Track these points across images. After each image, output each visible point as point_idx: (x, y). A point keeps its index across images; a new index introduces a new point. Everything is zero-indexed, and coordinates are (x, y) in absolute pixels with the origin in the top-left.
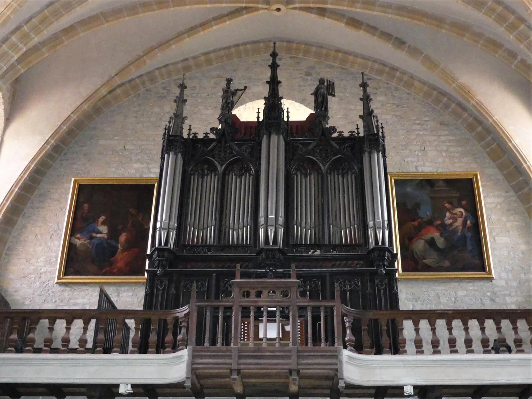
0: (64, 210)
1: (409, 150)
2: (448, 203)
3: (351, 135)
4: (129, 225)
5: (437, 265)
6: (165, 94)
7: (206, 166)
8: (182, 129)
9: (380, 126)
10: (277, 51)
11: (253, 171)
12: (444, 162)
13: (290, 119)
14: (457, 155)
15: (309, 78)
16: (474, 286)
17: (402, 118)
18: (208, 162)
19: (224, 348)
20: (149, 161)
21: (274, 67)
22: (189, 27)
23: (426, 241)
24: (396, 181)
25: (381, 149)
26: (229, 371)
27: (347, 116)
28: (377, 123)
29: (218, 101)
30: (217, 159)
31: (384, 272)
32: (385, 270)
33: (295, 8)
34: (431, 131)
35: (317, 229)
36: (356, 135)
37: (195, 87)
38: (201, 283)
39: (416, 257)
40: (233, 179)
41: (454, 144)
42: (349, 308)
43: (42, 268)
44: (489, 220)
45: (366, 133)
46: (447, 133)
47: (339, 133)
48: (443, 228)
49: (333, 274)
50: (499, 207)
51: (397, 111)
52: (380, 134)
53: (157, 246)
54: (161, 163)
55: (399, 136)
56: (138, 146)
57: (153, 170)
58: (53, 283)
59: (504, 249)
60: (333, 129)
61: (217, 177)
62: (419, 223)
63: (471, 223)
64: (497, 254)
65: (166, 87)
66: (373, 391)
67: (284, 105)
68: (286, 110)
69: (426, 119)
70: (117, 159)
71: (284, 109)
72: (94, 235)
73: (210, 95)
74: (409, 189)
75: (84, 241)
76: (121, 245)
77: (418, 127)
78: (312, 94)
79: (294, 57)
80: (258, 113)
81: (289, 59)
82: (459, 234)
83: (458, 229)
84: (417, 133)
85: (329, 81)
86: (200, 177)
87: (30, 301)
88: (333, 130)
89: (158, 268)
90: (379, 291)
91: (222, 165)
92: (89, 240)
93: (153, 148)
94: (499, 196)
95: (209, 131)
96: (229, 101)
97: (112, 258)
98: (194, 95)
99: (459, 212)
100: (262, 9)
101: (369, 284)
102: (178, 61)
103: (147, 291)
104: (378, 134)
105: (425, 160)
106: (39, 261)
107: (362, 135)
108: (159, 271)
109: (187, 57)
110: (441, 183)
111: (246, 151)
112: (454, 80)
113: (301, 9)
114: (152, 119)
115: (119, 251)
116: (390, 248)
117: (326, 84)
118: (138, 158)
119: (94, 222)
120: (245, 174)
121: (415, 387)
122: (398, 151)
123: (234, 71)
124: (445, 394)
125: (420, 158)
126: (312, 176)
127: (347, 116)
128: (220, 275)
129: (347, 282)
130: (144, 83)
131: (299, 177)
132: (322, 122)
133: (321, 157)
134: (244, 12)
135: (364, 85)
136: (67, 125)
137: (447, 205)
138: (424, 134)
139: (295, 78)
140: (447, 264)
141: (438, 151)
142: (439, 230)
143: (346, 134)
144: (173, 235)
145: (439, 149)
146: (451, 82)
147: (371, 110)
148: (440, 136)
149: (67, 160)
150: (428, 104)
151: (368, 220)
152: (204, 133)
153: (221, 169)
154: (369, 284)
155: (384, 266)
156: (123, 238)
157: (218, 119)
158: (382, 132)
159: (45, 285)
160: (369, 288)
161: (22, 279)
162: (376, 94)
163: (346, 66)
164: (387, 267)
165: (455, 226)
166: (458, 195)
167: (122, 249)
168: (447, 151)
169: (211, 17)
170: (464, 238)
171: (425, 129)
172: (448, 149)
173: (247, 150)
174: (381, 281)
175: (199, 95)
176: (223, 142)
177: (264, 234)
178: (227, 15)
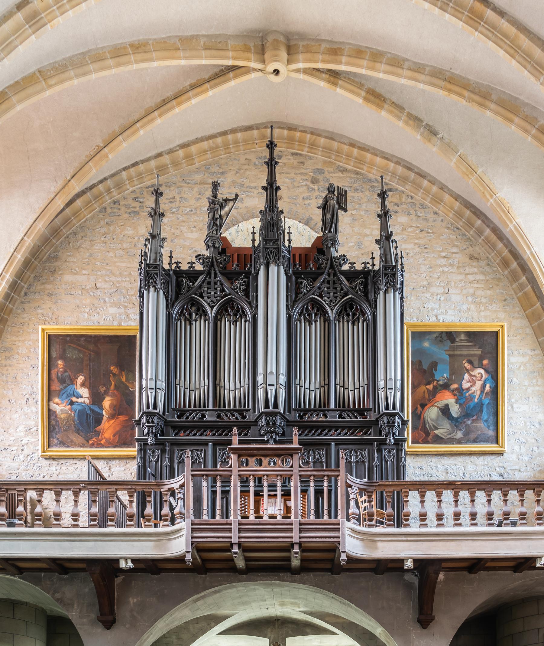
0: (36, 368)
1: (430, 292)
2: (468, 363)
3: (365, 267)
4: (112, 387)
5: (449, 436)
6: (137, 209)
7: (194, 308)
8: (161, 255)
9: (399, 256)
10: (275, 141)
11: (249, 317)
12: (468, 309)
13: (294, 245)
14: (484, 301)
15: (316, 187)
16: (484, 460)
17: (425, 248)
18: (194, 303)
19: (224, 521)
20: (126, 304)
21: (271, 164)
22: (159, 100)
23: (440, 409)
24: (413, 333)
25: (398, 286)
26: (229, 544)
27: (360, 244)
28: (397, 251)
29: (204, 218)
30: (206, 298)
31: (393, 441)
32: (394, 438)
33: (298, 71)
34: (458, 267)
35: (322, 390)
36: (371, 268)
37: (174, 198)
38: (197, 453)
39: (427, 427)
40: (226, 325)
41: (482, 286)
42: (354, 478)
43: (22, 439)
44: (510, 382)
45: (382, 264)
46: (476, 270)
47: (350, 265)
48: (460, 393)
49: (339, 443)
50: (522, 368)
51: (420, 238)
52: (399, 267)
53: (145, 410)
54: (140, 304)
55: (421, 273)
56: (112, 283)
57: (132, 316)
58: (38, 456)
59: (520, 419)
60: (344, 258)
61: (207, 322)
62: (433, 385)
63: (490, 387)
64: (513, 424)
65: (138, 197)
66: (372, 566)
67: (285, 222)
68: (287, 231)
69: (454, 250)
70: (88, 301)
71: (285, 229)
72: (74, 399)
73: (193, 210)
74: (426, 344)
75: (64, 407)
76: (106, 411)
77: (443, 261)
78: (318, 208)
79: (297, 154)
80: (254, 233)
81: (292, 157)
82: (476, 400)
83: (475, 394)
84: (442, 269)
85: (341, 188)
86: (188, 322)
87: (17, 477)
88: (344, 260)
89: (148, 436)
90: (386, 462)
91: (212, 308)
92: (69, 406)
93: (130, 286)
94: (523, 355)
95: (194, 260)
96: (217, 216)
97: (98, 428)
98: (174, 210)
99: (479, 373)
100: (255, 70)
101: (376, 455)
102: (150, 157)
103: (139, 462)
104: (395, 266)
105: (447, 307)
106: (18, 430)
107: (377, 268)
108: (149, 440)
109: (160, 151)
110: (463, 337)
111: (240, 289)
112: (492, 193)
113: (306, 71)
114: (125, 245)
115: (105, 418)
116: (401, 413)
117: (336, 193)
118: (114, 300)
119: (73, 384)
120: (240, 319)
121: (416, 561)
122: (418, 294)
123: (222, 173)
124: (443, 568)
125: (442, 304)
126: (318, 323)
127: (360, 244)
128: (216, 444)
129: (353, 452)
130: (109, 191)
131: (303, 324)
132: (330, 247)
133: (328, 298)
134: (231, 74)
135: (383, 195)
136: (22, 253)
137: (466, 365)
138: (450, 271)
139: (298, 187)
140: (459, 435)
141: (463, 295)
142: (455, 395)
143: (359, 267)
144: (161, 395)
145: (464, 292)
146: (488, 197)
147: (390, 233)
148: (468, 274)
149: (29, 302)
150: (458, 228)
151: (379, 380)
152: (189, 263)
153: (211, 313)
154: (376, 455)
155: (394, 434)
156: (107, 403)
157: (204, 242)
158: (401, 264)
159: (29, 458)
160: (376, 459)
161: (4, 451)
162: (397, 212)
163: (362, 169)
164: (396, 436)
165: (472, 391)
166: (479, 352)
167: (107, 416)
168: (473, 295)
169: (187, 84)
170: (480, 404)
171: (451, 265)
172: (475, 293)
173: (241, 287)
174: (389, 452)
175: (180, 211)
176: (213, 276)
177: (263, 396)
178: (209, 81)
